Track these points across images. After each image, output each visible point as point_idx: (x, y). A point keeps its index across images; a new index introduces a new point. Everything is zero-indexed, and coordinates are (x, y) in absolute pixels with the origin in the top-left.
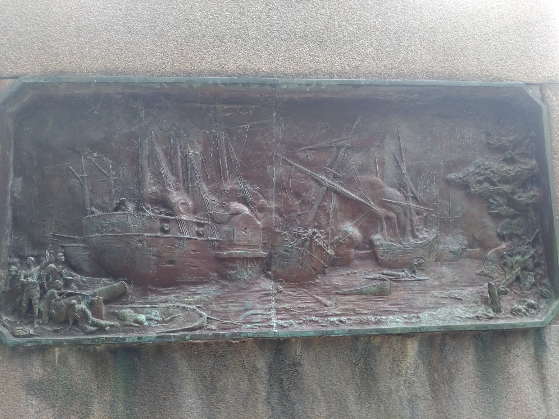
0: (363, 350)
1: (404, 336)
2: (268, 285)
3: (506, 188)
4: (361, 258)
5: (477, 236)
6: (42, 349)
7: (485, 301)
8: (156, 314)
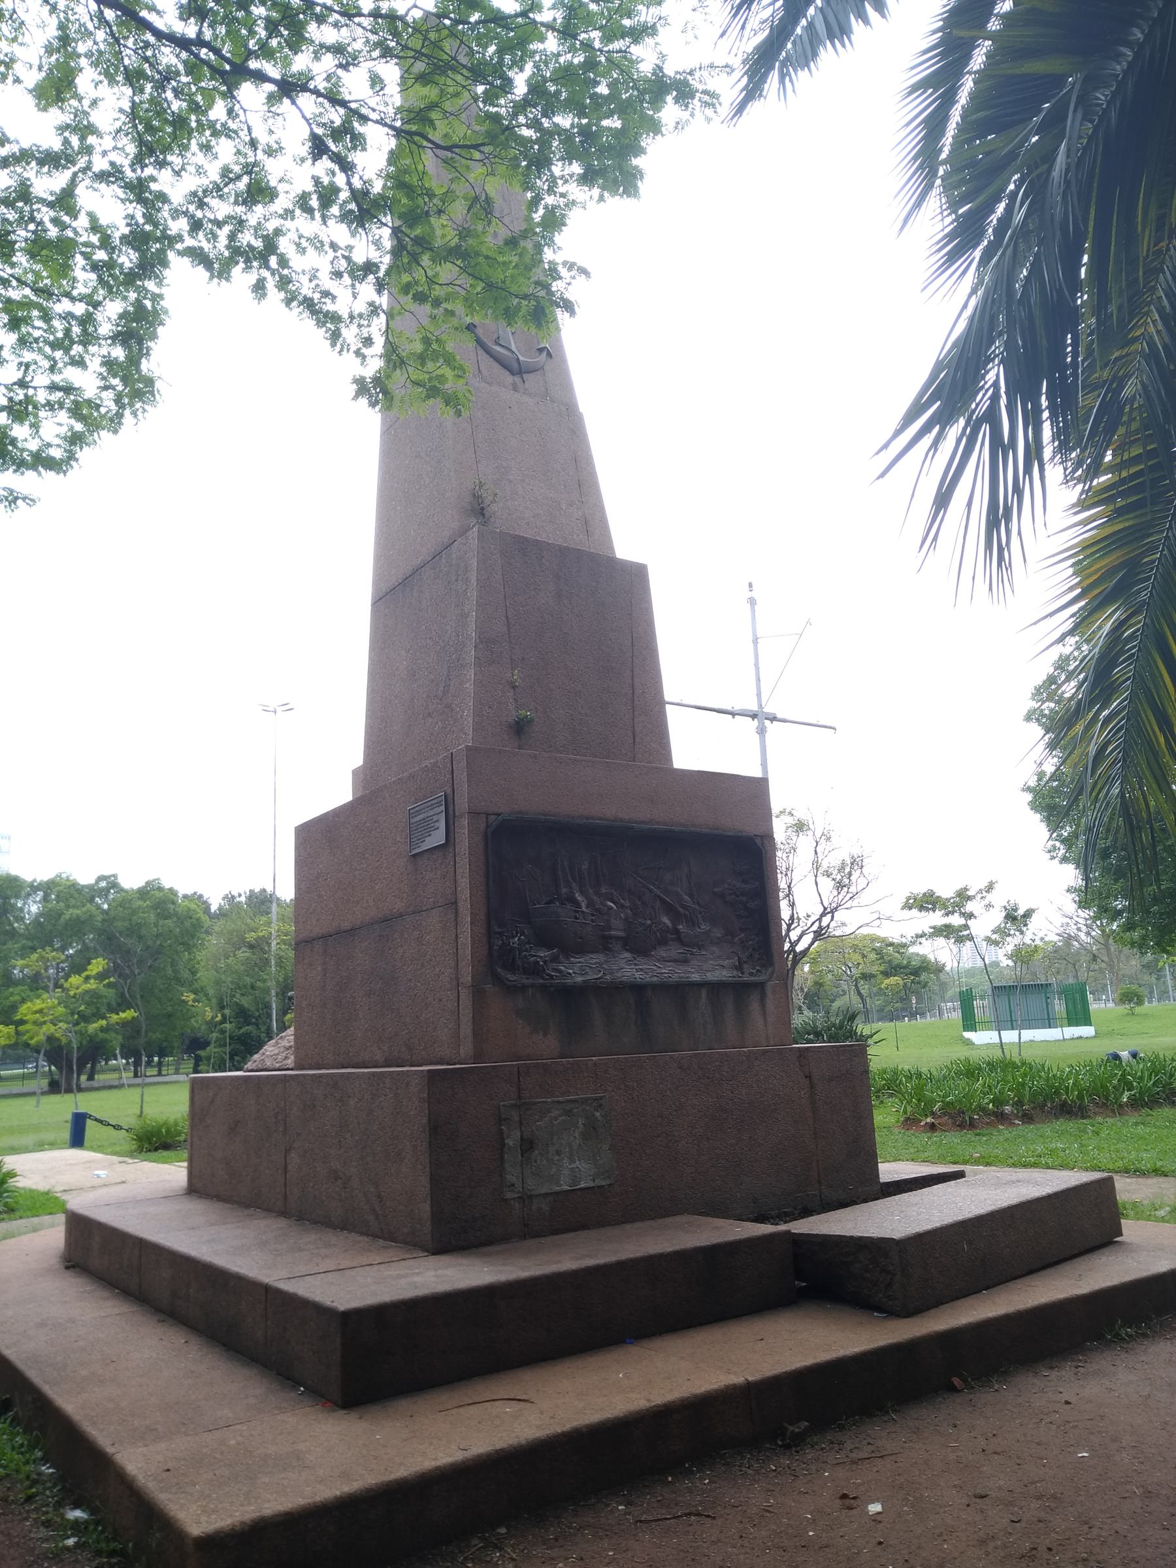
0: (680, 991)
1: (700, 985)
2: (627, 955)
3: (744, 899)
4: (672, 940)
5: (1154, 976)
6: (524, 988)
7: (736, 968)
8: (577, 970)
